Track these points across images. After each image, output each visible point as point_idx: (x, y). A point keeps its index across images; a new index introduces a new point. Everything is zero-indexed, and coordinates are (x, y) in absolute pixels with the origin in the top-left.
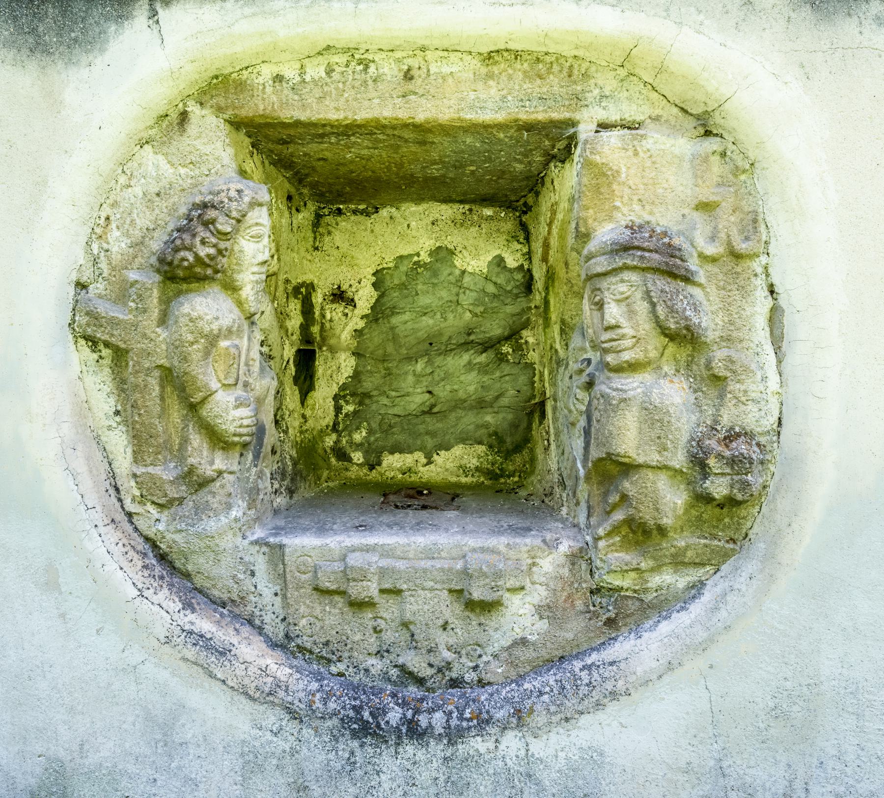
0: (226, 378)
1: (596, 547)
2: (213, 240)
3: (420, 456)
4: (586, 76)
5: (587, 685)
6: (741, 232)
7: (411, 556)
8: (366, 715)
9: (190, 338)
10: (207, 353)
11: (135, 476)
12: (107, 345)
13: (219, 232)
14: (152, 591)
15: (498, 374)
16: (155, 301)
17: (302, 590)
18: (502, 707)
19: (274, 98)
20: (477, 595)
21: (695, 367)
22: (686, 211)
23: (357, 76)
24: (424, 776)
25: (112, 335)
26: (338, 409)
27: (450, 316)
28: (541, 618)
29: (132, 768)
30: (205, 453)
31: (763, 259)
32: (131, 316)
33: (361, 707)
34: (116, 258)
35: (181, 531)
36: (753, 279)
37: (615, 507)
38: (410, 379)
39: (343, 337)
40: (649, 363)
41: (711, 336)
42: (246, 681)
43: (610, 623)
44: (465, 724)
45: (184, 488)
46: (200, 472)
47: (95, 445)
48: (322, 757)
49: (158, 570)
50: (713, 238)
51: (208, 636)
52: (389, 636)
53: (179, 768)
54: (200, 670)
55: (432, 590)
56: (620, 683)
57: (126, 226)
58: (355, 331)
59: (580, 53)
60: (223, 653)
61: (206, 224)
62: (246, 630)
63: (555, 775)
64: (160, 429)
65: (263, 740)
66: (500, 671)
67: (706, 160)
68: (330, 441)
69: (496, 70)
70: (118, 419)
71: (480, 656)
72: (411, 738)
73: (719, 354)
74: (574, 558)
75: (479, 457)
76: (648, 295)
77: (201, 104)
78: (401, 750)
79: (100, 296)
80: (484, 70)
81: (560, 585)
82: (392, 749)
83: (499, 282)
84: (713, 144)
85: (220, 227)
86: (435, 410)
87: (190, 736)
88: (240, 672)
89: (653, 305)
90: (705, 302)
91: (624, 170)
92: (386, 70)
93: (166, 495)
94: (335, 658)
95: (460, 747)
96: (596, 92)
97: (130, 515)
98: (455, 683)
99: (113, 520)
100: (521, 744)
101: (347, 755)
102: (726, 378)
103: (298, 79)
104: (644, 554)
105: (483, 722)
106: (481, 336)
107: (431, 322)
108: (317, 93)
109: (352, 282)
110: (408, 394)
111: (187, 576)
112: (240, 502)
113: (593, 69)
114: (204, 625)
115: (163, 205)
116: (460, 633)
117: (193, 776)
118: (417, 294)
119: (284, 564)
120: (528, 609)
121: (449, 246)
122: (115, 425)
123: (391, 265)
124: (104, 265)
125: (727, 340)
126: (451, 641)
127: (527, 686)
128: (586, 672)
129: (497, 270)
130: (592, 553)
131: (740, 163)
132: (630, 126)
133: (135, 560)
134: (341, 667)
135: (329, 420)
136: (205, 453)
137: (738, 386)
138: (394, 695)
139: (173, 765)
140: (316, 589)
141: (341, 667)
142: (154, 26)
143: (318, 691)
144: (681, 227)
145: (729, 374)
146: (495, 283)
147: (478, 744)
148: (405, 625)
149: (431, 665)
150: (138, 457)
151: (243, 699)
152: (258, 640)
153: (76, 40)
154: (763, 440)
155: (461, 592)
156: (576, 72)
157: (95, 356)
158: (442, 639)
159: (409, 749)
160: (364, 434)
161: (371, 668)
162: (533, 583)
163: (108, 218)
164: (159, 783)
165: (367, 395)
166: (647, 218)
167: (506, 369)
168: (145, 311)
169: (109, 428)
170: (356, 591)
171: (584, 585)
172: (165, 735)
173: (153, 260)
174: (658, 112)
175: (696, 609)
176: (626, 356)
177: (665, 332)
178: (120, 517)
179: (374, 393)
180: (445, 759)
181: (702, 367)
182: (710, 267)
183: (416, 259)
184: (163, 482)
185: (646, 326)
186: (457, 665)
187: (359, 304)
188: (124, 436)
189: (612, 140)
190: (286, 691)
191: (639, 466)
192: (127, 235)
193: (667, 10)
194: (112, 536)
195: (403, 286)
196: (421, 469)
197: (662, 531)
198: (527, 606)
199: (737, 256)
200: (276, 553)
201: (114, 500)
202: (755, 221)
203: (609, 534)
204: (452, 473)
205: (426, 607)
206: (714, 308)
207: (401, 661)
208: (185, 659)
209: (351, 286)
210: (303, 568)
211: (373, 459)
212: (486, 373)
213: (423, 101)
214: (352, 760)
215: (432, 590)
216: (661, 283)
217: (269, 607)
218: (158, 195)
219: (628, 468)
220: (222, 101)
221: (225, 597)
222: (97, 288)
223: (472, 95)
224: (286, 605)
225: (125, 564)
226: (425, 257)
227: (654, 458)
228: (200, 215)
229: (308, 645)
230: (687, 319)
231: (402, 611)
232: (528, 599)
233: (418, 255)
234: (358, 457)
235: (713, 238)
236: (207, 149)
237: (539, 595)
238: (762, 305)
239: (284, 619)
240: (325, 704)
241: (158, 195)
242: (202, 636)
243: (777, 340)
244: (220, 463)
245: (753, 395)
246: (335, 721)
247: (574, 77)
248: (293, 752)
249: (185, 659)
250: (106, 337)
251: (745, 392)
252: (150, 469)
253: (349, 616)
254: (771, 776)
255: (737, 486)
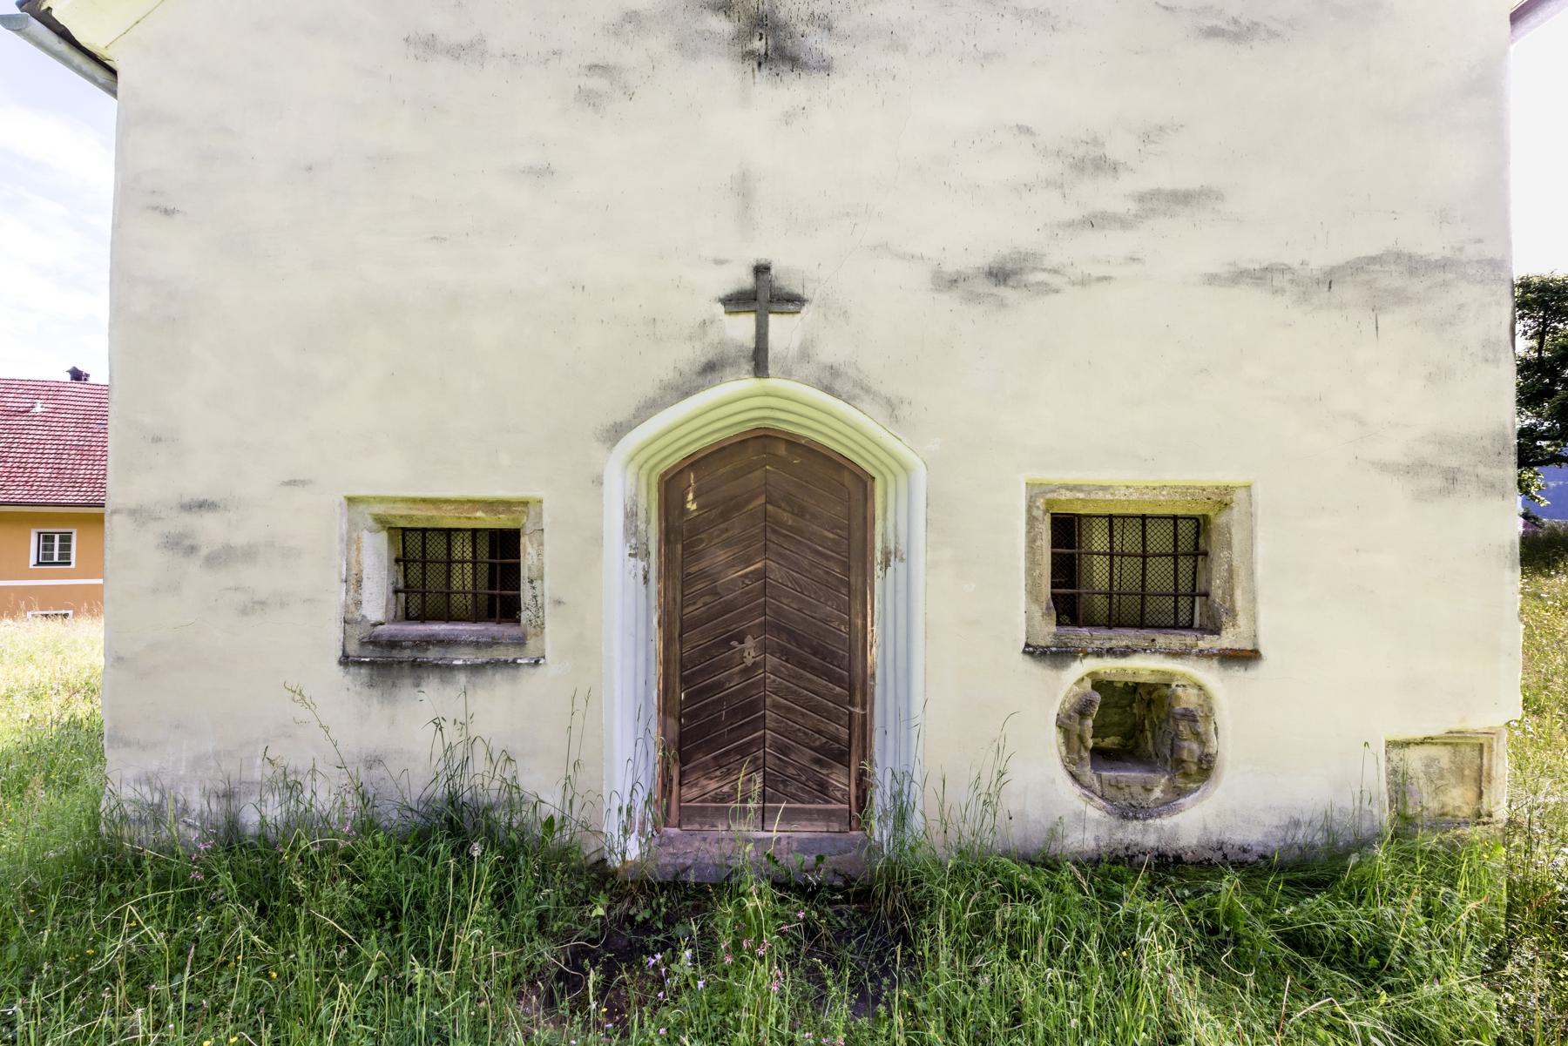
24: (1138, 828)
60: (1092, 799)
73: (1204, 737)
125: (1206, 734)
132: (1184, 686)
147: (1150, 821)
159: (1135, 822)
175: (1199, 792)
185: (1189, 732)
219: (1184, 761)
237: (1161, 787)
238: (1213, 726)
243: (1216, 734)
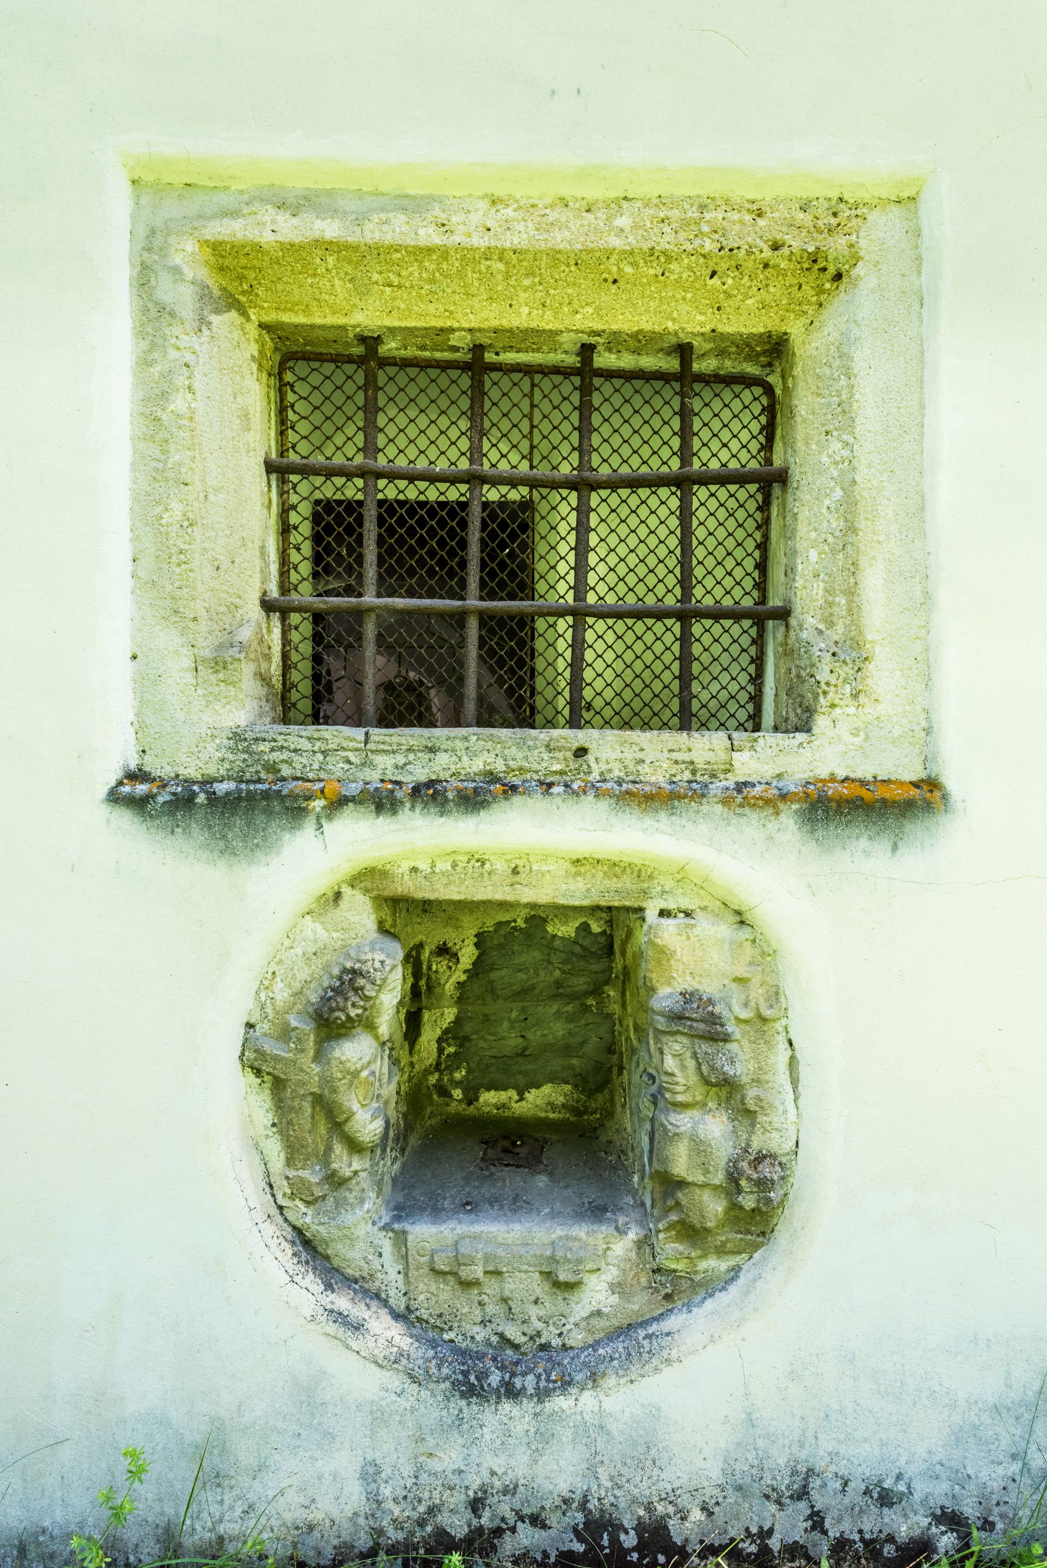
0: (364, 1099)
1: (657, 1237)
2: (362, 1003)
3: (513, 1094)
4: (651, 877)
5: (648, 1353)
6: (767, 1000)
7: (510, 1242)
8: (472, 1378)
9: (339, 1075)
10: (351, 1083)
11: (287, 1178)
12: (268, 1074)
13: (366, 996)
14: (300, 1276)
15: (583, 1022)
16: (312, 1044)
17: (421, 1271)
18: (581, 1370)
19: (410, 883)
20: (562, 1277)
21: (733, 1102)
22: (726, 982)
23: (476, 870)
25: (275, 1068)
26: (441, 1051)
27: (542, 973)
28: (613, 1293)
29: (280, 1425)
30: (345, 1158)
31: (784, 1022)
32: (291, 1055)
33: (468, 1372)
34: (279, 1004)
35: (324, 1224)
36: (776, 1035)
37: (671, 1209)
38: (506, 1025)
39: (447, 987)
40: (697, 1103)
41: (745, 1079)
42: (376, 1352)
43: (668, 1297)
44: (551, 1385)
45: (327, 1187)
46: (341, 1174)
47: (254, 1151)
48: (436, 1414)
49: (304, 1256)
50: (746, 1005)
51: (346, 1313)
52: (491, 1309)
53: (320, 1424)
54: (339, 1343)
55: (526, 1272)
56: (674, 1351)
57: (289, 979)
58: (458, 983)
59: (647, 863)
60: (357, 1327)
61: (356, 990)
62: (374, 1304)
63: (621, 1427)
64: (310, 1140)
65: (389, 1400)
66: (580, 1337)
67: (741, 945)
68: (433, 1079)
69: (583, 869)
70: (275, 1129)
71: (564, 1325)
72: (509, 1398)
73: (751, 1093)
74: (640, 1244)
75: (565, 1095)
76: (695, 1056)
77: (353, 886)
78: (500, 1407)
79: (265, 1035)
80: (574, 869)
81: (628, 1266)
82: (493, 1407)
83: (585, 944)
84: (745, 933)
85: (367, 993)
86: (527, 1053)
87: (329, 1397)
88: (371, 1344)
89: (699, 1064)
90: (740, 1053)
91: (679, 949)
92: (498, 867)
93: (313, 1195)
94: (447, 1327)
95: (547, 1404)
96: (659, 888)
97: (281, 1208)
98: (545, 1347)
99: (269, 1216)
100: (595, 1402)
101: (456, 1412)
102: (756, 1112)
103: (429, 870)
104: (694, 1245)
105: (566, 1384)
106: (569, 990)
107: (524, 977)
108: (444, 880)
109: (456, 941)
110: (503, 1038)
111: (327, 1258)
112: (371, 1194)
113: (656, 873)
114: (342, 1302)
115: (319, 962)
116: (549, 1307)
117: (331, 1430)
118: (513, 953)
119: (406, 1247)
120: (603, 1286)
121: (542, 915)
122: (271, 1134)
123: (491, 929)
124: (269, 1010)
125: (757, 1081)
126: (542, 1313)
127: (601, 1351)
128: (648, 1341)
129: (583, 934)
130: (654, 1240)
131: (766, 949)
132: (688, 914)
133: (287, 1249)
134: (451, 1335)
135: (432, 1060)
136: (345, 1158)
137: (765, 1118)
138: (494, 1359)
139: (315, 1422)
140: (433, 1270)
141: (451, 1335)
142: (320, 836)
143: (434, 1358)
144: (722, 995)
145: (758, 1109)
146: (581, 946)
147: (560, 1403)
148: (505, 1300)
149: (524, 1334)
150: (290, 1162)
151: (373, 1366)
152: (384, 1312)
153: (257, 845)
154: (784, 1160)
155: (550, 1273)
156: (643, 874)
157: (259, 1081)
158: (534, 1312)
159: (507, 1406)
160: (463, 1073)
161: (476, 1336)
162: (607, 1264)
163: (274, 973)
164: (302, 1437)
165: (466, 1039)
166: (697, 986)
167: (590, 1018)
168: (303, 1051)
169: (267, 1136)
170: (465, 1273)
171: (648, 1266)
172: (309, 1397)
173: (311, 1010)
174: (705, 903)
176: (680, 1098)
177: (707, 1082)
178: (274, 1211)
179: (475, 1037)
180: (535, 1414)
181: (738, 1102)
182: (743, 1026)
183: (513, 924)
184: (311, 1184)
185: (693, 1079)
186: (545, 1332)
187: (462, 959)
188: (279, 1143)
189: (670, 928)
190: (408, 1359)
191: (689, 1184)
192: (290, 986)
193: (711, 840)
194: (270, 1229)
195: (500, 947)
196: (514, 1105)
197: (707, 1231)
198: (602, 1283)
199: (764, 1020)
200: (401, 1239)
201: (269, 1196)
202: (777, 993)
203: (667, 1230)
204: (541, 1109)
205: (522, 1286)
206: (747, 1057)
207: (500, 1329)
208: (327, 1335)
209: (455, 944)
210: (422, 1252)
211: (471, 1095)
212: (572, 1021)
213: (526, 889)
214: (461, 1416)
215: (526, 1272)
216: (705, 1047)
217: (394, 1283)
218: (315, 954)
220: (369, 885)
221: (357, 1274)
222: (263, 1027)
223: (564, 887)
224: (407, 1281)
225: (279, 1255)
226: (521, 923)
227: (700, 1179)
228: (351, 980)
229: (425, 1317)
230: (724, 1073)
231: (502, 1289)
232: (604, 1277)
233: (515, 921)
234: (457, 1093)
235: (746, 1005)
236: (356, 919)
237: (611, 1274)
239: (405, 1294)
240: (439, 1370)
241: (315, 954)
242: (340, 1314)
243: (795, 1082)
244: (356, 1165)
245: (776, 1125)
246: (448, 1384)
247: (642, 878)
248: (413, 1410)
249: (327, 1335)
250: (270, 1070)
251: (770, 1123)
252: (301, 1173)
253: (459, 1292)
254: (788, 1426)
255: (762, 1201)
